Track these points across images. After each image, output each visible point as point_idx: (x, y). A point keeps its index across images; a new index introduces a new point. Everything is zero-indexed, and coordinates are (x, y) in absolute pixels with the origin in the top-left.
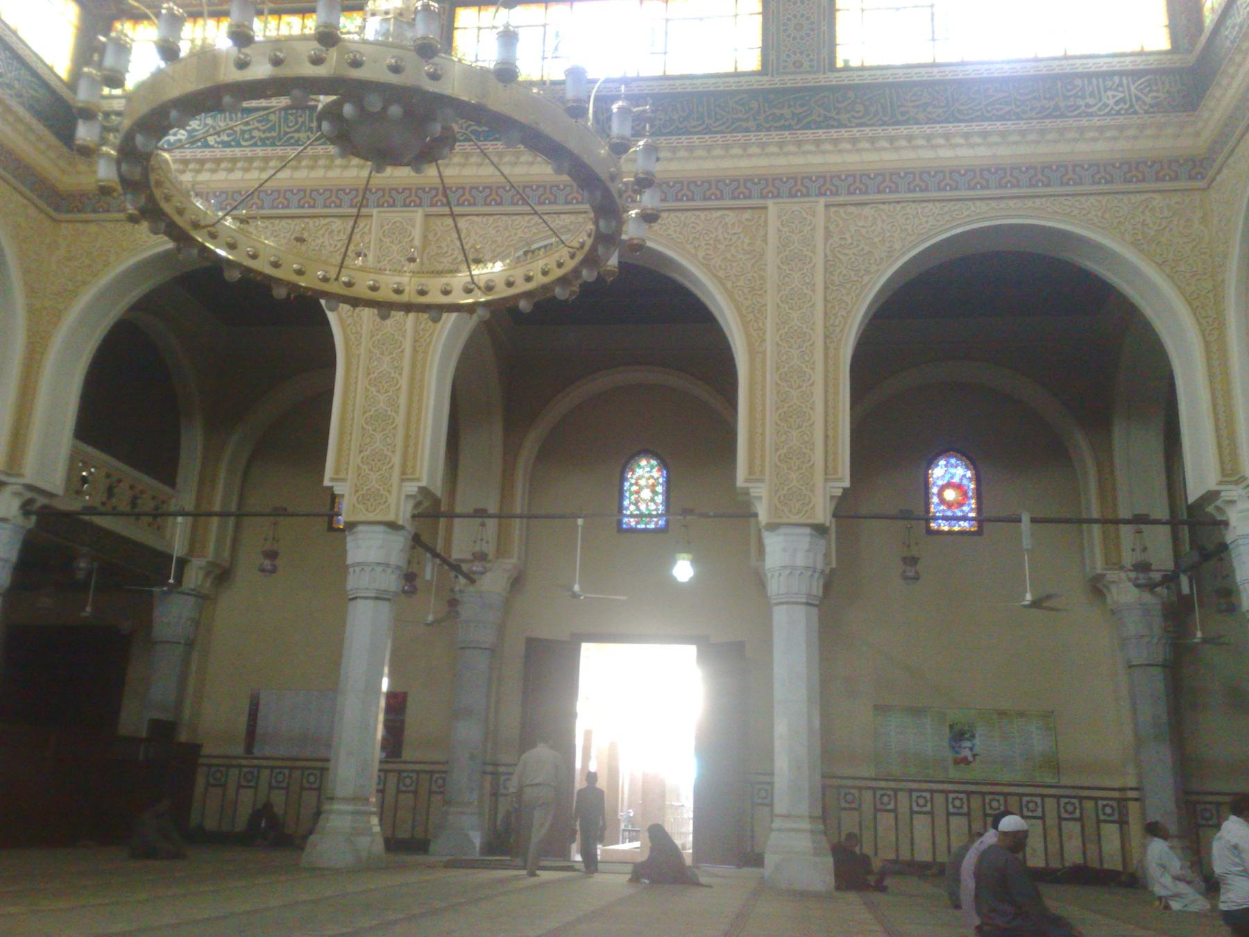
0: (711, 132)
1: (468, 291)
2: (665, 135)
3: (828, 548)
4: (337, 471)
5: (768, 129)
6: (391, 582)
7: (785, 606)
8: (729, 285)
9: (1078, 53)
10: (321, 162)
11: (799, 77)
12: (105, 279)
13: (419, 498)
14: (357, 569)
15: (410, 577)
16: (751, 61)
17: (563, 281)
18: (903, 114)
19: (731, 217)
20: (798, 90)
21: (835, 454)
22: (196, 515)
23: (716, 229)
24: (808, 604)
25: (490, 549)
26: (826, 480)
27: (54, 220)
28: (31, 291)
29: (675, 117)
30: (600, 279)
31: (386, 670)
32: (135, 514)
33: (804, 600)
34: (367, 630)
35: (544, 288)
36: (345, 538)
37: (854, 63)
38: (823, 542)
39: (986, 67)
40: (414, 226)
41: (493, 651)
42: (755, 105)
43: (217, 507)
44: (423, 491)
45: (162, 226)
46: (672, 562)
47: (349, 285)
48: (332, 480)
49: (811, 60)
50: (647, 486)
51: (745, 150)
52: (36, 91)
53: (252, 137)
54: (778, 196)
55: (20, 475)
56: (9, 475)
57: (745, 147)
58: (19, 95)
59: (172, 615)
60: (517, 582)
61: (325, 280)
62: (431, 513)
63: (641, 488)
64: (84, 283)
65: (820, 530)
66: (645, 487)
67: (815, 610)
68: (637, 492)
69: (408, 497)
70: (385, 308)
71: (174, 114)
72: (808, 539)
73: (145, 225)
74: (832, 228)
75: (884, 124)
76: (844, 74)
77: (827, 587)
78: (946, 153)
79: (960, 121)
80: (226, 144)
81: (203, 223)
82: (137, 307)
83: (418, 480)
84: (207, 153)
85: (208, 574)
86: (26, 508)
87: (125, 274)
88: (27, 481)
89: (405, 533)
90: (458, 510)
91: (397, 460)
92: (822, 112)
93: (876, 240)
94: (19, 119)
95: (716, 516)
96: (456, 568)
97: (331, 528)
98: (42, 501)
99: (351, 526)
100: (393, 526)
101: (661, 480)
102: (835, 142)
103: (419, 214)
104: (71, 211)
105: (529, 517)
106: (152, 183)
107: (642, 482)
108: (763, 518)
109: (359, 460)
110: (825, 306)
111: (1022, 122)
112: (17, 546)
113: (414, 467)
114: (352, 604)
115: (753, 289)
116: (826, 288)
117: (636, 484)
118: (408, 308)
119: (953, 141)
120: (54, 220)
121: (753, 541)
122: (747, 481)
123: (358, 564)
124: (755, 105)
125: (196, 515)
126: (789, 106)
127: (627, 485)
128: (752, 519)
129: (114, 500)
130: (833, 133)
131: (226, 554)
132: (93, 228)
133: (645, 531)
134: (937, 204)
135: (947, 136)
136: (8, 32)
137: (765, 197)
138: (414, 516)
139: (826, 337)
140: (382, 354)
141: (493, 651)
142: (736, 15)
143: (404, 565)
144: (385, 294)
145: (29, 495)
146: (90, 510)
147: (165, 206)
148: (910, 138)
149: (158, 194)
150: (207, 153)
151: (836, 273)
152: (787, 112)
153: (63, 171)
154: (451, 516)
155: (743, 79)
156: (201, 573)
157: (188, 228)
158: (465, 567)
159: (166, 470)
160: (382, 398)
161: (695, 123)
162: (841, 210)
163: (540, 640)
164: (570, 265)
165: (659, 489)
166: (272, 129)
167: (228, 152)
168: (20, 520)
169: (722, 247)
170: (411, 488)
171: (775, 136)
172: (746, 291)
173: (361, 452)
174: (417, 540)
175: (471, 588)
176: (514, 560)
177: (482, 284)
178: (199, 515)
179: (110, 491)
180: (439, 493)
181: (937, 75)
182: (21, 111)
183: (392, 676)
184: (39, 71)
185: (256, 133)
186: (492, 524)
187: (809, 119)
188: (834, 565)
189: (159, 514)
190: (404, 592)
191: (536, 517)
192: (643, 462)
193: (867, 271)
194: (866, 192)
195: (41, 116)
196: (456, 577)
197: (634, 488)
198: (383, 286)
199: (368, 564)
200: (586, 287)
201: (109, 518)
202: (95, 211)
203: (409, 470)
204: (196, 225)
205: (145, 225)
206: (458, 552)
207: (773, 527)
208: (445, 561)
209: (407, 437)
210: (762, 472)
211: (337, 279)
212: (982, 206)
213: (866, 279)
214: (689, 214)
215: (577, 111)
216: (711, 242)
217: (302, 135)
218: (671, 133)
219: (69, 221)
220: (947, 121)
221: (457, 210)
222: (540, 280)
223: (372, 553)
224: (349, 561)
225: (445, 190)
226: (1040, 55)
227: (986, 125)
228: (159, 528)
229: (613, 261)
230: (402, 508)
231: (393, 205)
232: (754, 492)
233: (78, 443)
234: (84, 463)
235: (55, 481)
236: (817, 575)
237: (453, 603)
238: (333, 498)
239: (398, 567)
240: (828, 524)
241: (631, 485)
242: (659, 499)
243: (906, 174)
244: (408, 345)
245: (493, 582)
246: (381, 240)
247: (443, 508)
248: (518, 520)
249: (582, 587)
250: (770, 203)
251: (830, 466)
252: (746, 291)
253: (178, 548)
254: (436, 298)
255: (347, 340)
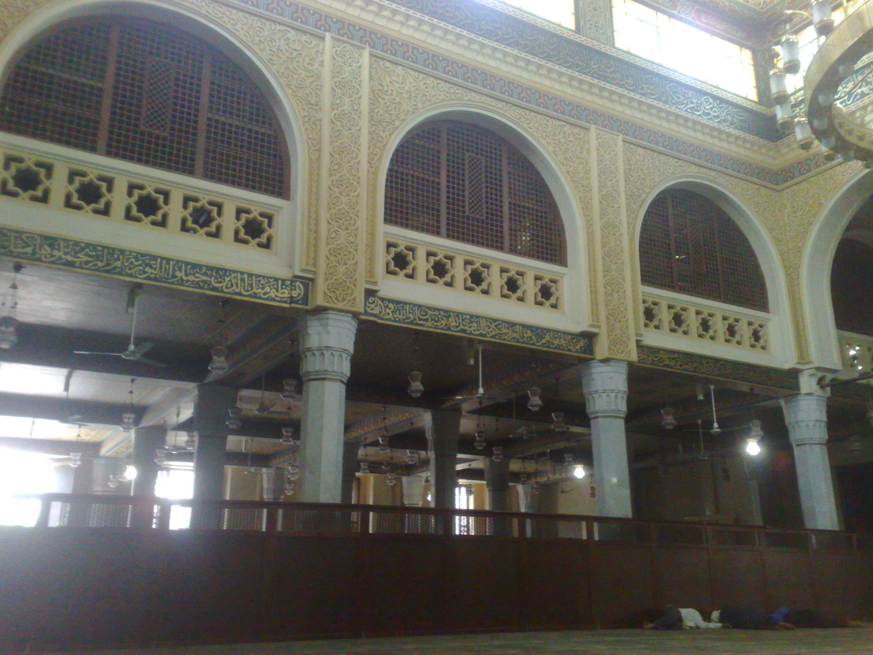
9: (528, 10)
27: (777, 191)
28: (778, 241)
45: (852, 153)
52: (741, 116)
58: (732, 123)
64: (810, 224)
71: (841, 69)
73: (839, 159)
82: (850, 227)
87: (836, 206)
88: (815, 365)
94: (737, 138)
98: (829, 376)
106: (837, 126)
120: (777, 191)
132: (803, 186)
136: (714, 89)
145: (820, 374)
147: (849, 138)
149: (842, 132)
153: (774, 158)
168: (819, 392)
182: (737, 132)
205: (839, 159)
219: (787, 188)
226: (523, 8)
233: (841, 331)
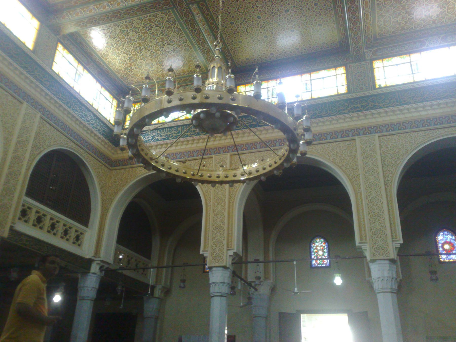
0: (330, 116)
1: (243, 175)
2: (314, 118)
3: (397, 268)
4: (205, 248)
5: (353, 112)
6: (225, 289)
7: (382, 293)
8: (344, 168)
10: (195, 142)
11: (362, 93)
12: (126, 188)
13: (234, 256)
14: (214, 285)
15: (233, 288)
16: (343, 90)
17: (277, 168)
18: (404, 101)
19: (341, 144)
20: (363, 97)
21: (395, 230)
22: (158, 268)
23: (336, 149)
24: (392, 292)
25: (262, 275)
26: (393, 241)
28: (103, 193)
29: (317, 112)
30: (291, 167)
31: (226, 328)
32: (136, 269)
33: (390, 291)
34: (218, 307)
35: (270, 171)
36: (209, 275)
37: (383, 85)
38: (395, 266)
39: (435, 81)
40: (227, 159)
41: (266, 318)
42: (346, 104)
43: (165, 265)
44: (235, 253)
45: (141, 159)
46: (333, 277)
47: (201, 176)
48: (203, 251)
49: (366, 87)
50: (320, 250)
51: (344, 120)
53: (173, 136)
54: (359, 135)
55: (99, 257)
56: (96, 257)
57: (344, 119)
59: (151, 307)
60: (273, 290)
61: (193, 175)
62: (239, 262)
63: (318, 251)
64: (120, 189)
65: (393, 261)
66: (319, 248)
67: (395, 295)
68: (317, 252)
69: (230, 256)
70: (213, 183)
72: (388, 265)
74: (382, 144)
75: (397, 105)
76: (380, 90)
77: (399, 287)
78: (423, 113)
79: (428, 101)
80: (164, 139)
81: (153, 158)
83: (233, 249)
84: (159, 143)
85: (162, 292)
86: (101, 269)
89: (229, 270)
90: (249, 260)
91: (225, 242)
92: (373, 104)
93: (400, 147)
95: (349, 258)
96: (250, 284)
97: (204, 272)
98: (106, 266)
99: (210, 268)
100: (225, 267)
101: (326, 247)
102: (379, 114)
103: (228, 155)
104: (115, 166)
105: (275, 262)
107: (319, 248)
108: (368, 258)
109: (212, 244)
110: (383, 173)
111: (453, 99)
112: (98, 282)
113: (231, 245)
114: (212, 298)
115: (353, 169)
116: (383, 167)
117: (316, 249)
118: (221, 183)
119: (426, 109)
121: (366, 269)
122: (360, 243)
123: (214, 283)
124: (346, 104)
125: (158, 268)
126: (360, 103)
127: (312, 250)
128: (365, 259)
129: (130, 265)
130: (378, 111)
131: (168, 283)
133: (322, 267)
134: (423, 132)
135: (423, 107)
137: (354, 136)
138: (232, 264)
139: (385, 185)
140: (218, 204)
141: (266, 318)
142: (336, 75)
143: (230, 283)
144: (214, 178)
145: (102, 264)
146: (122, 268)
148: (408, 109)
149: (140, 148)
150: (159, 143)
151: (386, 161)
152: (359, 105)
153: (113, 154)
154: (247, 263)
155: (341, 96)
156: (160, 291)
157: (149, 160)
158: (253, 284)
159: (148, 255)
160: (219, 220)
161: (324, 113)
162: (385, 137)
163: (285, 313)
164: (279, 162)
165: (325, 250)
166: (178, 133)
167: (165, 142)
169: (339, 155)
170: (231, 253)
171: (355, 114)
172: (351, 170)
173: (212, 240)
174: (234, 274)
175: (256, 293)
176: (271, 281)
177: (247, 172)
178: (158, 268)
179: (129, 262)
180: (241, 254)
181: (416, 86)
183: (228, 329)
184: (105, 122)
185: (174, 135)
186: (261, 265)
187: (368, 107)
188: (401, 278)
189: (145, 269)
190: (231, 294)
191: (278, 262)
192: (318, 240)
193: (399, 159)
194: (394, 130)
195: (106, 137)
196: (250, 288)
197: (315, 250)
198: (213, 176)
199: (217, 283)
200: (285, 170)
201: (127, 271)
202: (123, 165)
203: (230, 246)
204: (151, 159)
206: (250, 278)
207: (373, 261)
208: (246, 282)
209: (228, 234)
210: (366, 239)
211: (197, 174)
212: (442, 131)
213: (398, 162)
214: (325, 145)
215: (245, 77)
216: (335, 154)
217: (189, 134)
218: (315, 118)
220: (422, 101)
221: (240, 152)
222: (268, 169)
223: (218, 278)
224: (210, 282)
225: (235, 145)
227: (438, 101)
228: (145, 275)
229: (295, 160)
230: (228, 261)
231: (220, 153)
232: (363, 248)
234: (120, 252)
235: (110, 260)
236: (394, 280)
237: (250, 298)
238: (204, 259)
239: (228, 284)
240: (396, 259)
241: (314, 249)
242: (326, 254)
243: (409, 122)
244: (227, 201)
245: (264, 290)
246: (216, 165)
247: (244, 260)
248: (271, 263)
249: (298, 290)
250: (356, 138)
251: (394, 235)
252: (351, 170)
253: (151, 281)
254: (231, 178)
255: (206, 200)
